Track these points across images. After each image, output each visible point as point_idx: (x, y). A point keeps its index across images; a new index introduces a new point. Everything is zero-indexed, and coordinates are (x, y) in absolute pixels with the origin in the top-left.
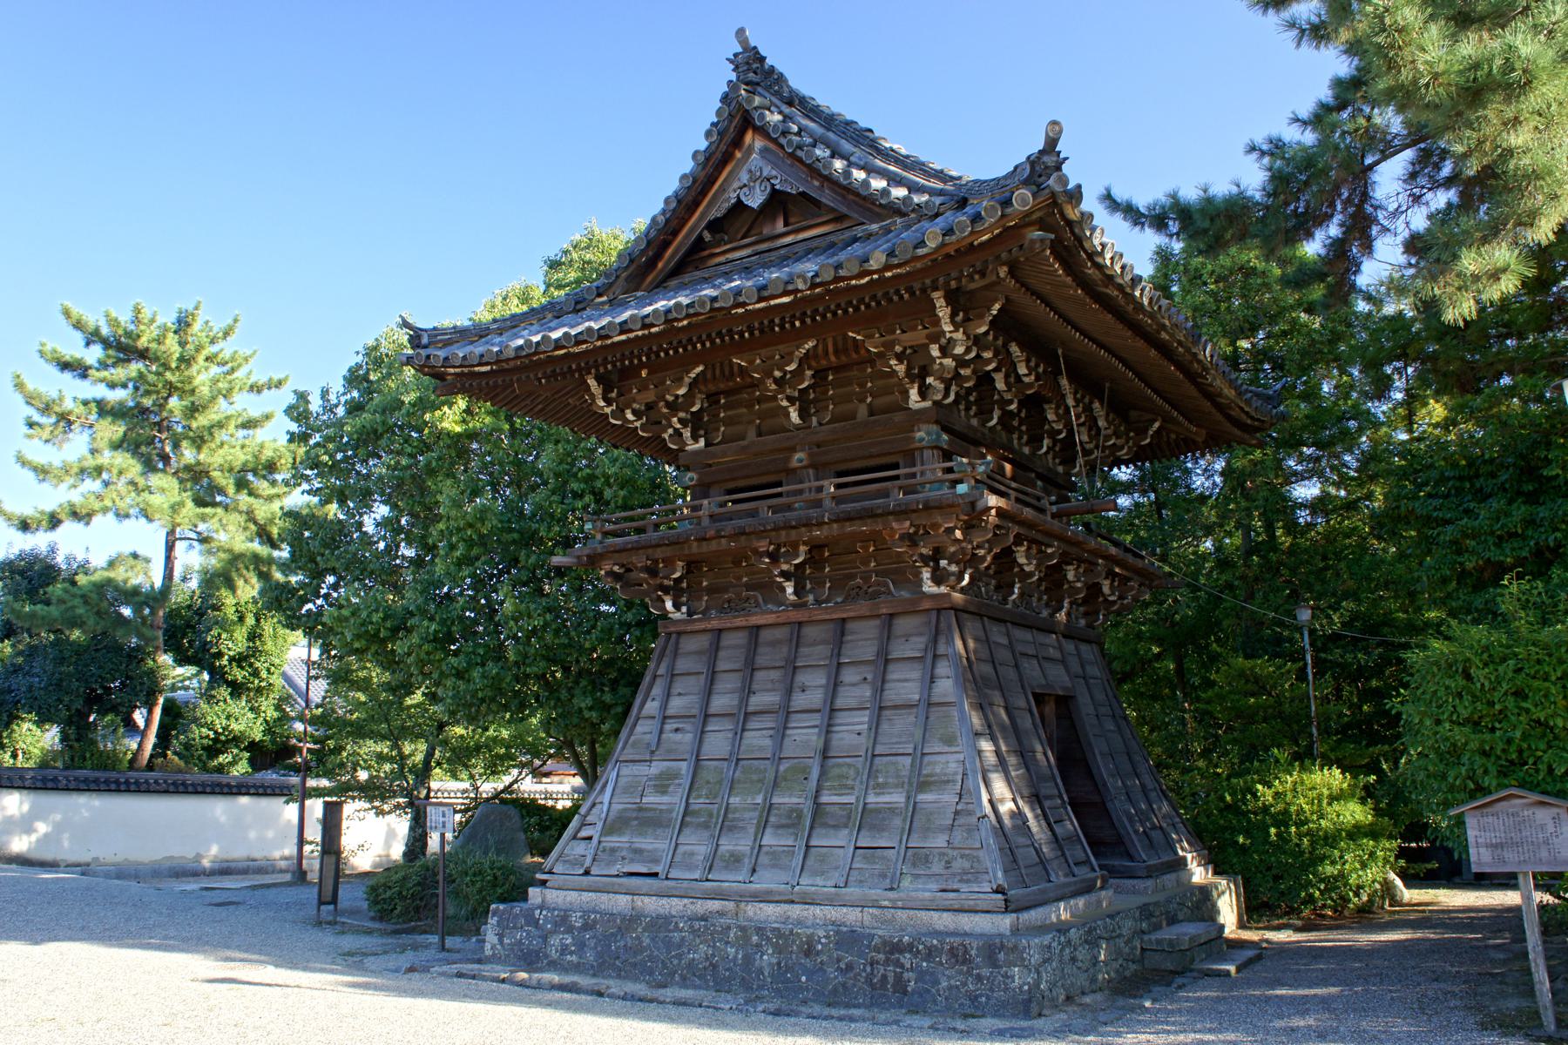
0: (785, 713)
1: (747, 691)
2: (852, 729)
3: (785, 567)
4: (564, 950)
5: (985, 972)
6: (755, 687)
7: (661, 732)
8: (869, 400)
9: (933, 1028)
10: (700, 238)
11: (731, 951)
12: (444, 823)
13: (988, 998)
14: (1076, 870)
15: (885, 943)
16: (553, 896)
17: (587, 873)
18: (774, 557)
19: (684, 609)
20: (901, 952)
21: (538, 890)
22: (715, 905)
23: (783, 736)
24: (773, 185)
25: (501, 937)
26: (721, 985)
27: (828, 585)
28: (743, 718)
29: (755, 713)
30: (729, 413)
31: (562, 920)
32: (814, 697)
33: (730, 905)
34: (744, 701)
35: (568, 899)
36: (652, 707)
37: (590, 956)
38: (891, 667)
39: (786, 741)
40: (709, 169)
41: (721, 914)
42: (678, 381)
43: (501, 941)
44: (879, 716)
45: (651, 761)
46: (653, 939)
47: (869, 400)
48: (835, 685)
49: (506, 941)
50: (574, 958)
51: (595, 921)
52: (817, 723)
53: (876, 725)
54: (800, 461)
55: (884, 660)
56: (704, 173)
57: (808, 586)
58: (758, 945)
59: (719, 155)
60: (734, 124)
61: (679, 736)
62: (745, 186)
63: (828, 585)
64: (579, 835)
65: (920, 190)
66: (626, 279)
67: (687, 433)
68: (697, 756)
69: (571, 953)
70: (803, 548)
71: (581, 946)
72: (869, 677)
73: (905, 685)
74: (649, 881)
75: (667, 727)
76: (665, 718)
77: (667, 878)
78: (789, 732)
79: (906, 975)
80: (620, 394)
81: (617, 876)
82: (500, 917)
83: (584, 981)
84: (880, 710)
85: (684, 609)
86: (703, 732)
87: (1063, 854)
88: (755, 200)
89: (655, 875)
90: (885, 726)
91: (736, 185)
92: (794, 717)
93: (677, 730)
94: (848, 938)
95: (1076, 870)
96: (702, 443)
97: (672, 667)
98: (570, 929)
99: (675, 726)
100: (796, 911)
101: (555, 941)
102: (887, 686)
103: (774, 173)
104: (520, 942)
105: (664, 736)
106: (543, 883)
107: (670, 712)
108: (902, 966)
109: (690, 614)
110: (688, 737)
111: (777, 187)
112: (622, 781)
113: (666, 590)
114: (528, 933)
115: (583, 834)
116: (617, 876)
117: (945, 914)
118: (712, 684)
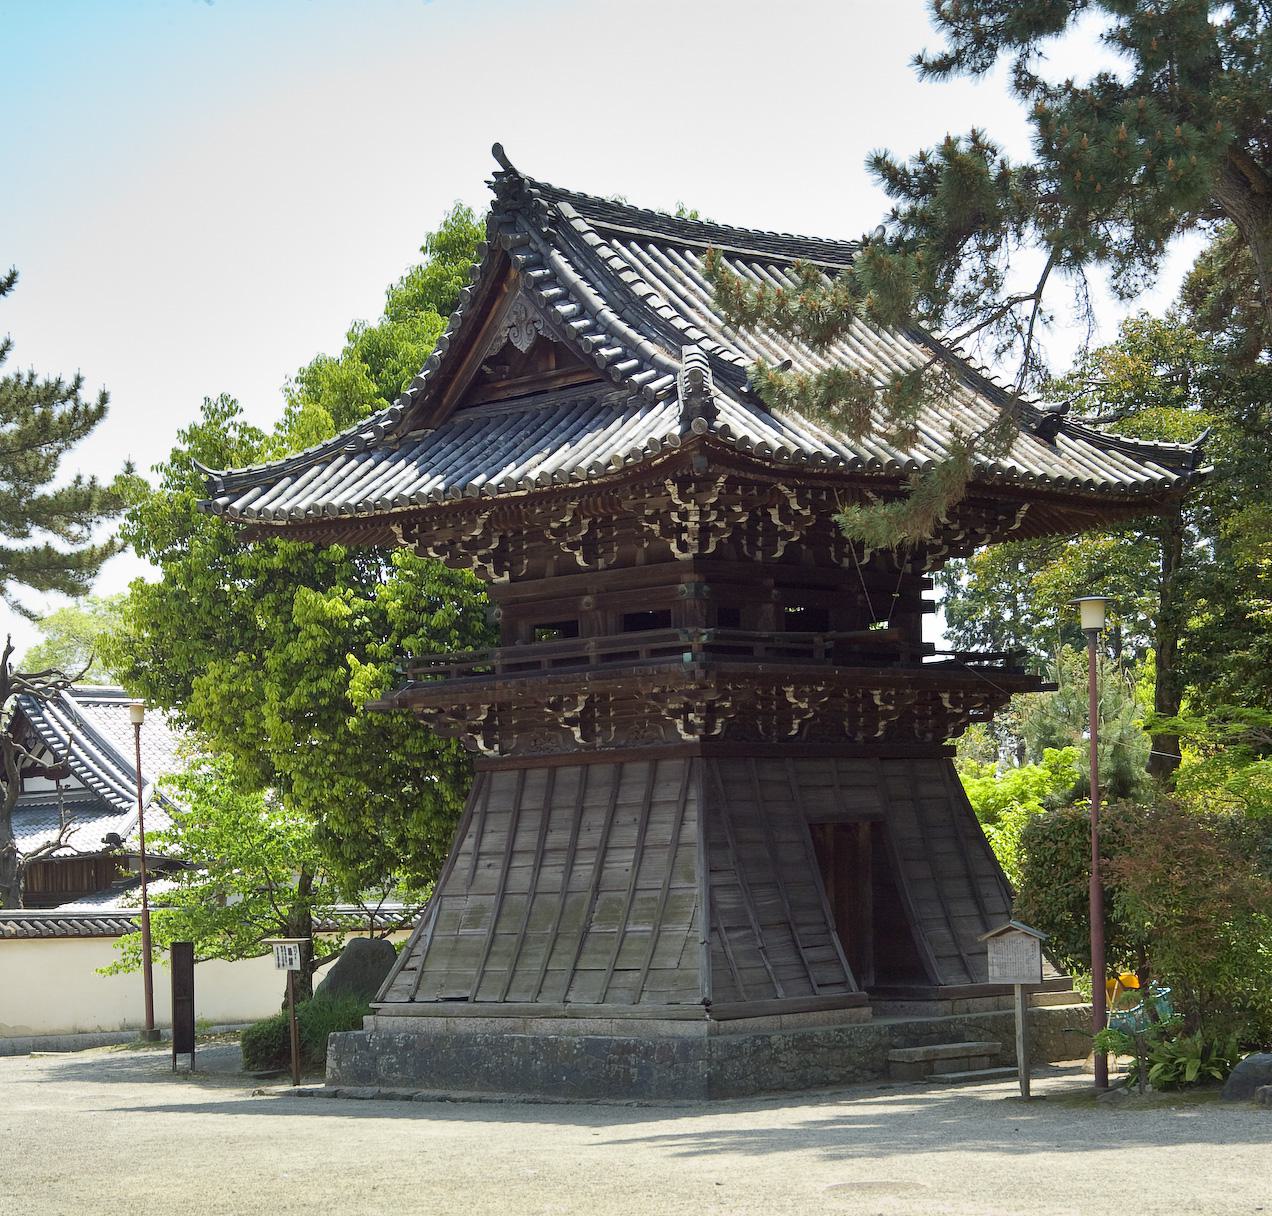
0: (573, 851)
1: (545, 829)
2: (621, 862)
3: (568, 715)
4: (390, 1068)
5: (681, 1065)
6: (551, 826)
7: (476, 867)
8: (646, 545)
9: (640, 1105)
10: (481, 372)
11: (515, 1059)
12: (291, 960)
13: (683, 1085)
14: (817, 989)
15: (618, 1045)
16: (384, 1022)
17: (412, 1000)
18: (556, 707)
19: (496, 747)
20: (629, 1053)
21: (371, 1017)
22: (509, 1023)
23: (571, 871)
24: (537, 330)
25: (339, 1061)
26: (508, 1086)
27: (613, 728)
28: (541, 854)
29: (519, 852)
30: (532, 545)
31: (388, 1043)
32: (590, 838)
33: (520, 1022)
34: (543, 838)
35: (396, 1024)
36: (469, 843)
37: (411, 1071)
38: (655, 810)
39: (574, 875)
40: (478, 307)
41: (513, 1030)
42: (473, 524)
43: (339, 1064)
44: (642, 854)
45: (467, 896)
46: (457, 1053)
47: (646, 545)
48: (610, 826)
49: (343, 1064)
50: (399, 1075)
51: (414, 1041)
52: (593, 860)
53: (639, 860)
54: (588, 604)
55: (649, 805)
56: (473, 311)
57: (598, 729)
58: (533, 1053)
59: (485, 293)
60: (497, 259)
61: (490, 872)
62: (513, 326)
63: (613, 728)
64: (407, 966)
65: (697, 326)
66: (412, 417)
67: (490, 568)
68: (504, 890)
69: (396, 1071)
70: (581, 699)
71: (403, 1062)
72: (639, 819)
73: (662, 829)
74: (461, 1004)
75: (481, 863)
76: (479, 854)
77: (475, 1002)
78: (575, 868)
79: (632, 1070)
80: (422, 531)
81: (437, 1001)
82: (337, 1045)
83: (402, 1091)
84: (641, 849)
85: (496, 747)
86: (509, 868)
87: (808, 976)
88: (523, 345)
89: (465, 999)
90: (646, 863)
91: (506, 323)
92: (549, 855)
93: (489, 866)
94: (593, 1046)
95: (817, 989)
96: (506, 577)
97: (485, 805)
98: (394, 1050)
99: (488, 862)
100: (567, 1024)
101: (383, 1060)
102: (650, 827)
103: (537, 316)
104: (355, 1064)
105: (479, 872)
106: (374, 1011)
107: (484, 848)
108: (629, 1064)
109: (502, 752)
110: (498, 872)
111: (541, 333)
112: (444, 913)
113: (475, 730)
114: (361, 1055)
115: (410, 965)
116: (437, 1001)
117: (666, 1022)
118: (518, 821)
